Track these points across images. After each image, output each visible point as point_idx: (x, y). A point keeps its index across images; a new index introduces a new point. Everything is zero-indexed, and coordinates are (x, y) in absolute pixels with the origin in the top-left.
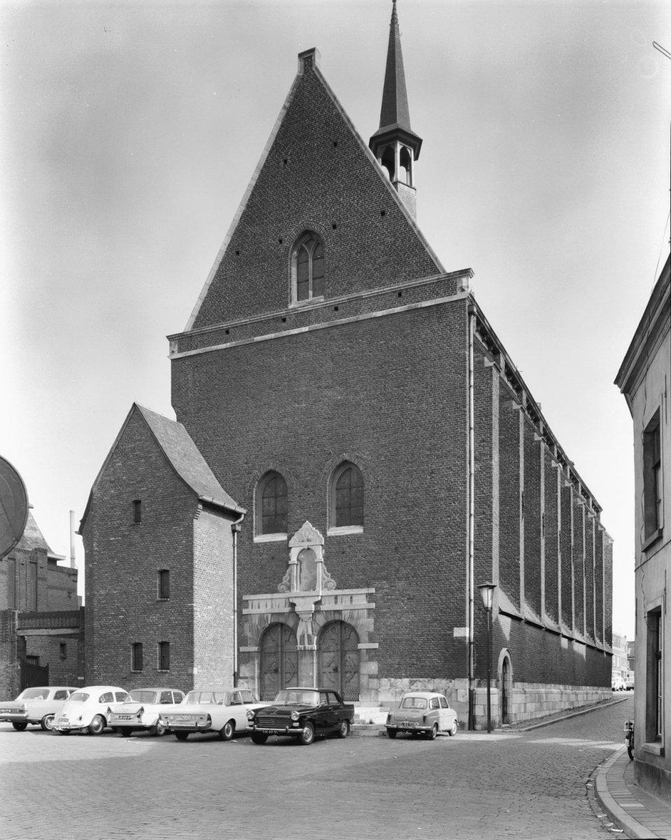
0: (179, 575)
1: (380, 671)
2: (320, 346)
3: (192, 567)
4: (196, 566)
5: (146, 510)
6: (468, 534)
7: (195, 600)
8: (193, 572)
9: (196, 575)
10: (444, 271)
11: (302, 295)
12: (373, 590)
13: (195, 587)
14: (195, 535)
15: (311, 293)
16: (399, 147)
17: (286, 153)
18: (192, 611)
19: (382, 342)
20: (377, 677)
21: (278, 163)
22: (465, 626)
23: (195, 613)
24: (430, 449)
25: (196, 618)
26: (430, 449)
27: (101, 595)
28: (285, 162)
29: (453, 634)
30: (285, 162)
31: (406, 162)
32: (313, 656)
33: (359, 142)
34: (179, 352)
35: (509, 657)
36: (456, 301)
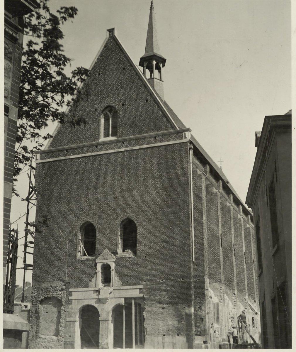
11: (106, 135)
12: (141, 287)
16: (154, 63)
17: (100, 71)
21: (96, 75)
28: (99, 74)
30: (99, 74)
31: (158, 68)
34: (40, 160)
35: (113, 266)
36: (183, 143)
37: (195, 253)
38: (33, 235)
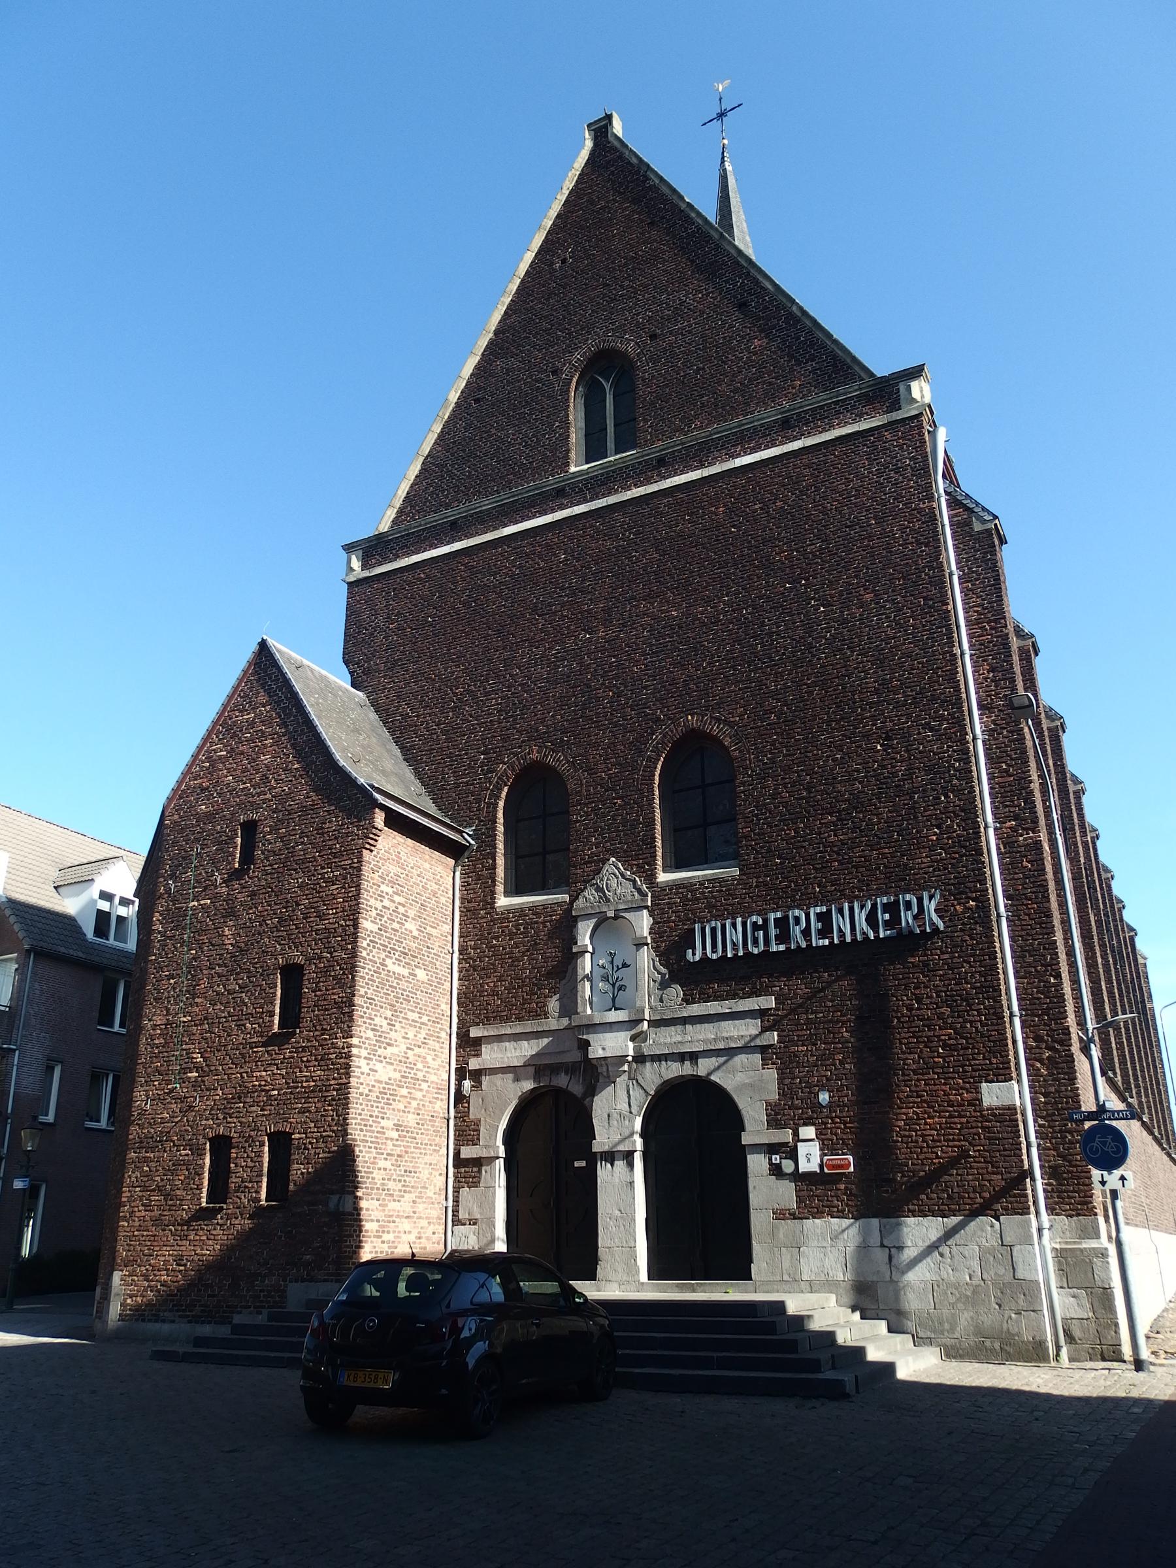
0: (325, 972)
1: (800, 1200)
2: (630, 528)
3: (354, 954)
4: (364, 954)
5: (268, 841)
6: (987, 860)
7: (356, 1030)
8: (354, 966)
9: (361, 972)
10: (872, 374)
13: (357, 1000)
14: (364, 885)
15: (611, 445)
18: (349, 1056)
19: (756, 507)
20: (794, 1217)
22: (1011, 1079)
23: (355, 1062)
24: (876, 692)
25: (356, 1072)
26: (876, 692)
27: (155, 1026)
29: (981, 1100)
30: (564, 261)
32: (631, 1165)
33: (693, 215)
37: (997, 845)
38: (857, 910)
